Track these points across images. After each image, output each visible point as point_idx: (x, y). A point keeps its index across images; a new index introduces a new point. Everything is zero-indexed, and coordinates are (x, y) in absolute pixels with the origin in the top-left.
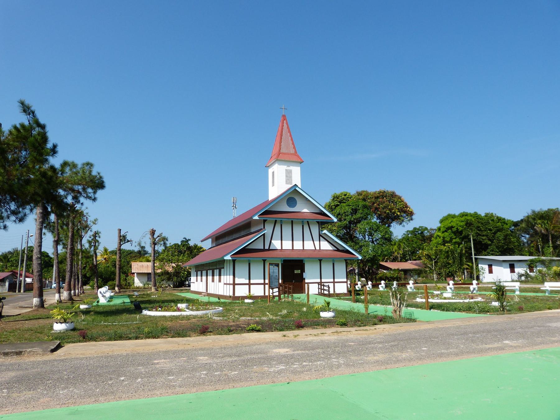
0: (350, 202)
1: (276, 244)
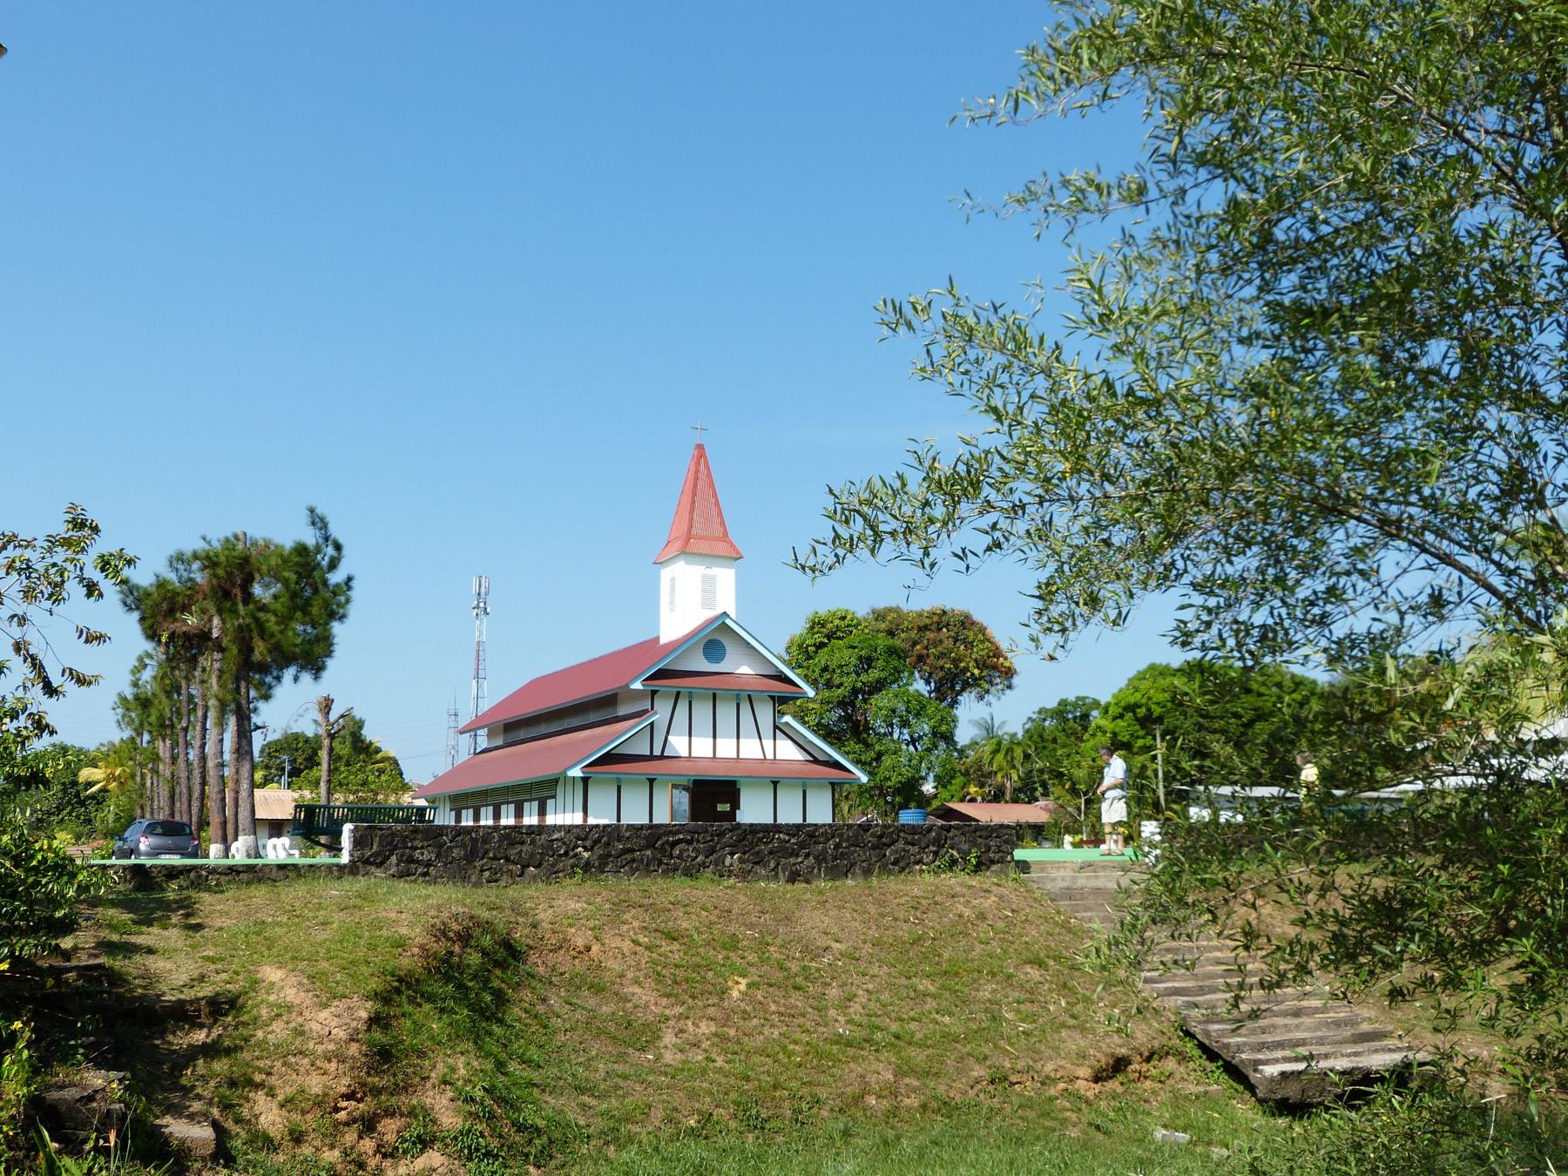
0: (854, 639)
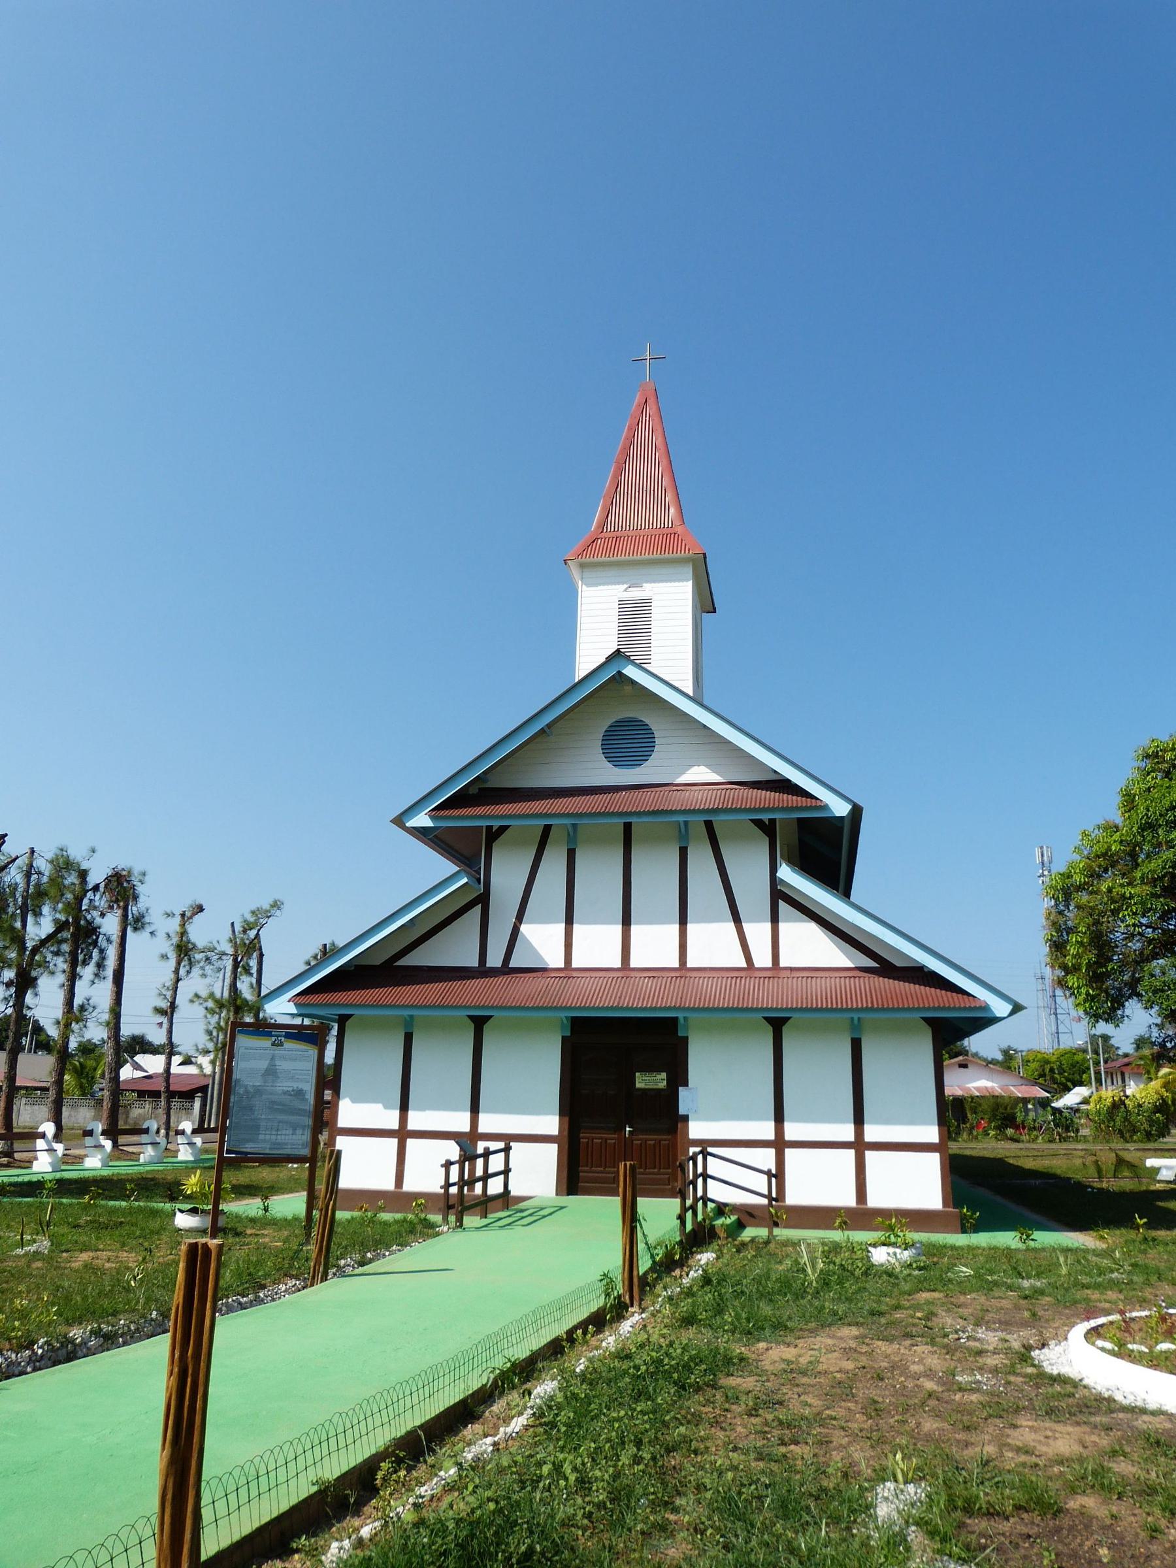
1: (543, 941)
